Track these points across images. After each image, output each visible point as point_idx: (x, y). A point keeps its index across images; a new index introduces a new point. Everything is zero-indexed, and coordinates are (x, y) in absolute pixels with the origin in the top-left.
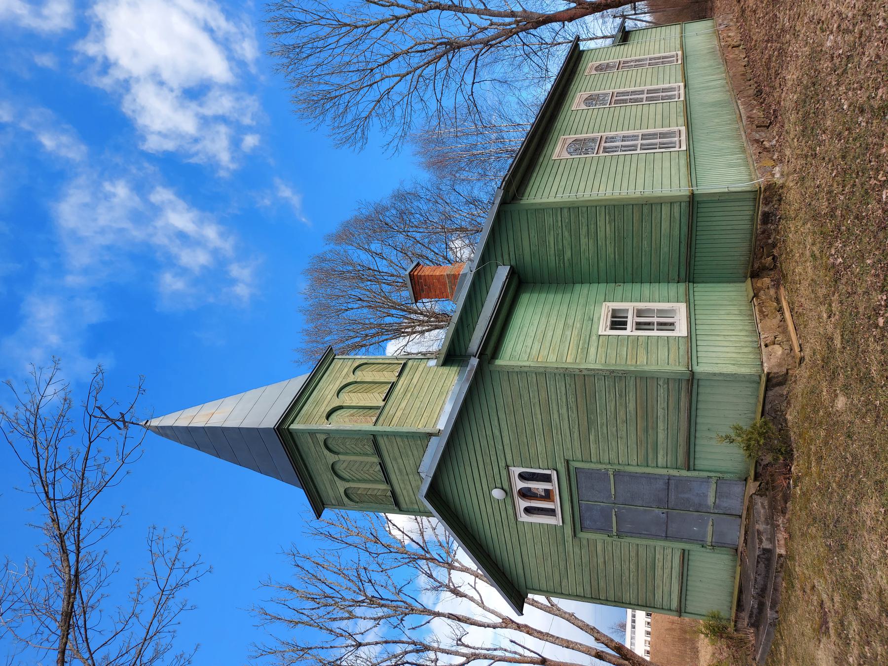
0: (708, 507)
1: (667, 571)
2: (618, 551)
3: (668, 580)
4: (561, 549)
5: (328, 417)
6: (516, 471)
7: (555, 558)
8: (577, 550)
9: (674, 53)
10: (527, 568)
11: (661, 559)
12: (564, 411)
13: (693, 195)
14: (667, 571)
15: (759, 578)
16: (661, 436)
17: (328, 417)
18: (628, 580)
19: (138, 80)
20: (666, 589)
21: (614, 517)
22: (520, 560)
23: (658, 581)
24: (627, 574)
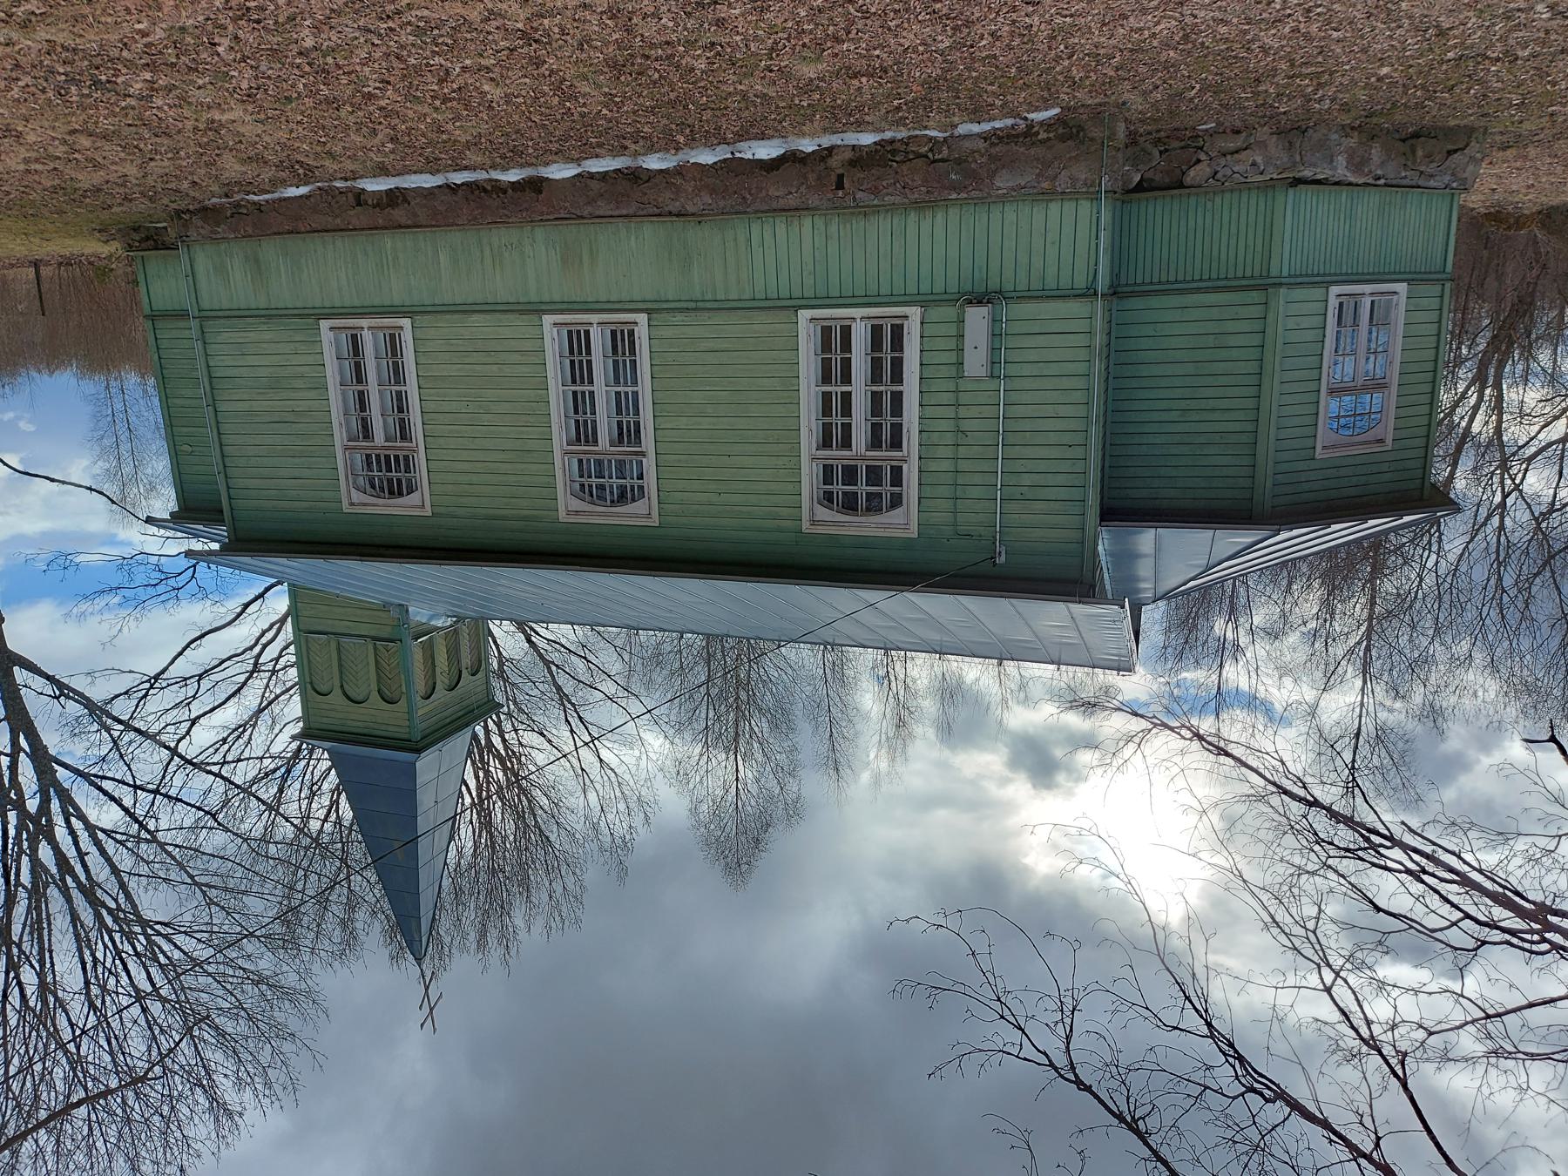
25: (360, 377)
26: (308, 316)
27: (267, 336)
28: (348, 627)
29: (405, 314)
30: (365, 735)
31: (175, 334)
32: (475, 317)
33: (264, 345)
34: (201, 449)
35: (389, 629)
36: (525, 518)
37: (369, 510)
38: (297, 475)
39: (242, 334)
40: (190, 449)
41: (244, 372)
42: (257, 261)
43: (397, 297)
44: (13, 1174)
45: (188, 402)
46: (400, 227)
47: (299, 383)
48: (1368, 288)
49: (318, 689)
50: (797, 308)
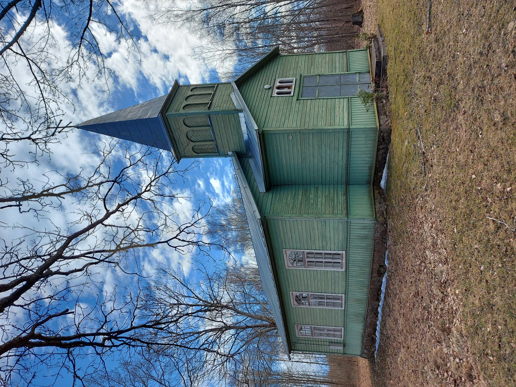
0: (357, 82)
1: (341, 108)
2: (318, 104)
3: (342, 113)
4: (289, 106)
5: (186, 100)
6: (278, 80)
7: (285, 110)
8: (297, 105)
9: (340, 295)
10: (267, 119)
11: (338, 104)
12: (303, 63)
13: (349, 129)
14: (341, 108)
15: (376, 46)
16: (337, 65)
17: (183, 108)
18: (321, 115)
19: (66, 221)
20: (341, 117)
21: (317, 91)
22: (265, 114)
23: (337, 113)
24: (321, 113)
25: (328, 298)
26: (347, 247)
27: (340, 237)
28: (218, 135)
29: (346, 271)
30: (171, 129)
31: (341, 140)
32: (344, 283)
33: (337, 236)
34: (291, 144)
35: (222, 150)
36: (289, 285)
37: (285, 256)
38: (293, 238)
39: (341, 231)
40: (291, 139)
41: (328, 229)
42: (366, 238)
43: (351, 269)
44: (2, 267)
45: (311, 142)
46: (372, 274)
47: (324, 243)
48: (344, 261)
49: (186, 123)
50: (345, 294)
